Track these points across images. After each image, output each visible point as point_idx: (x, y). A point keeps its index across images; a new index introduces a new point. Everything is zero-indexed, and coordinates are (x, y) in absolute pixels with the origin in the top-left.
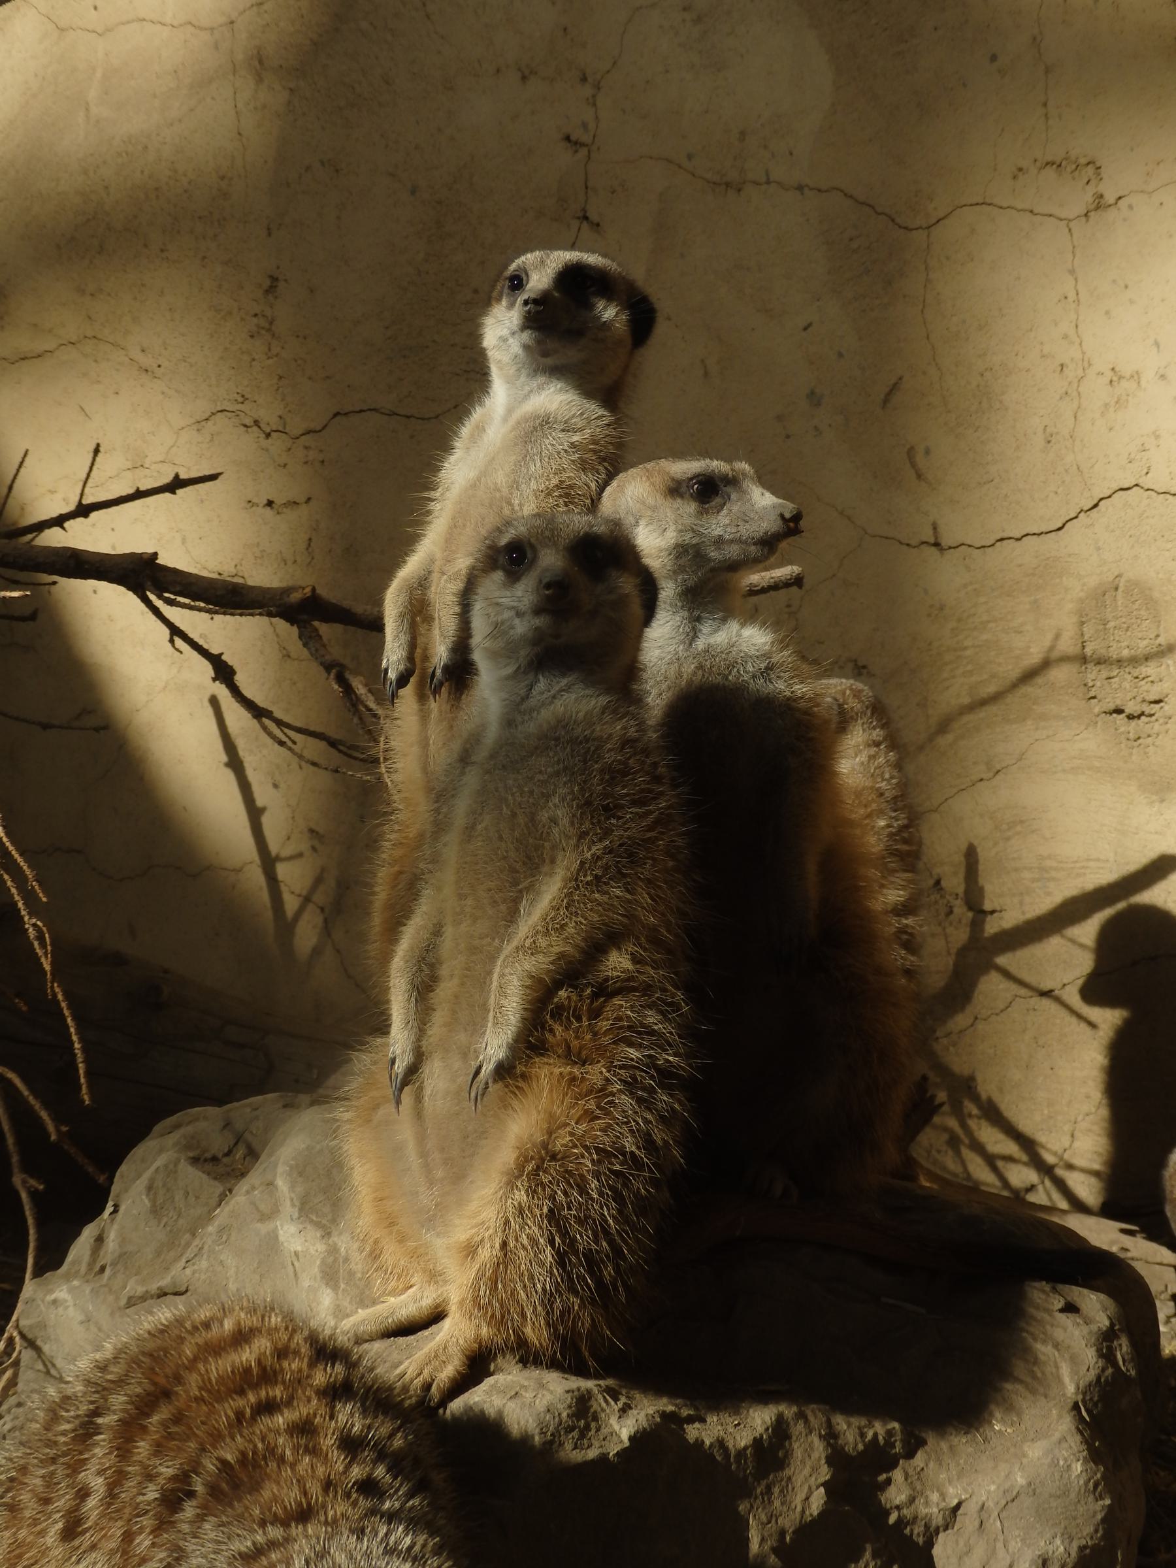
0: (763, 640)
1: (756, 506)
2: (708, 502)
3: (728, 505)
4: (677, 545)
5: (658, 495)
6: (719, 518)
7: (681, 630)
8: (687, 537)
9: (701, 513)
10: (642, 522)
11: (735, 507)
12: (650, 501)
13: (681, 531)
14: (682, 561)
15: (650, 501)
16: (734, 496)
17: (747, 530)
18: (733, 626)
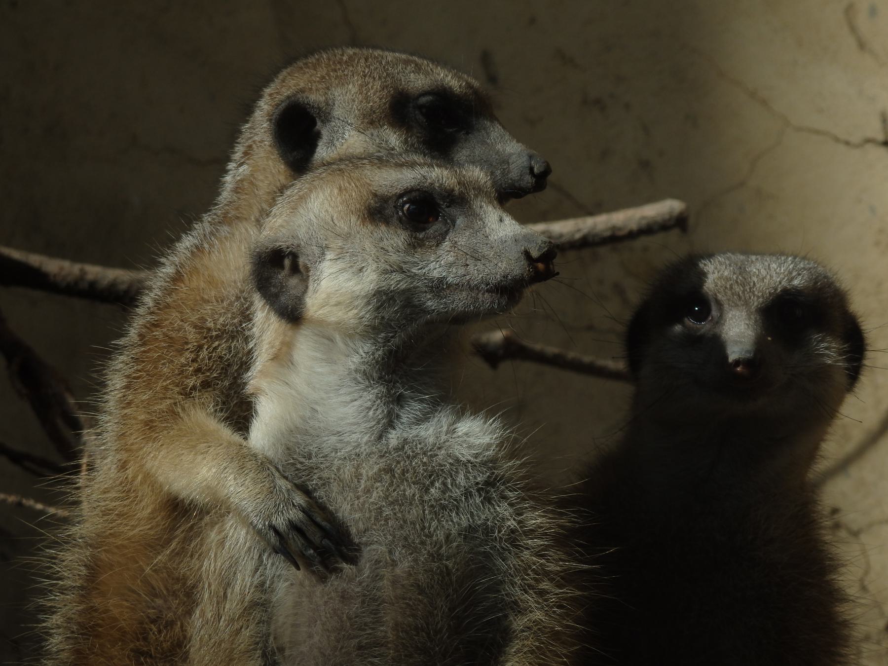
0: (486, 439)
1: (491, 238)
2: (424, 229)
3: (451, 235)
4: (378, 293)
5: (353, 219)
6: (440, 252)
7: (371, 413)
8: (395, 281)
9: (415, 245)
10: (330, 255)
11: (461, 238)
12: (342, 226)
13: (385, 272)
14: (387, 314)
15: (342, 226)
16: (460, 221)
17: (477, 272)
18: (443, 419)
